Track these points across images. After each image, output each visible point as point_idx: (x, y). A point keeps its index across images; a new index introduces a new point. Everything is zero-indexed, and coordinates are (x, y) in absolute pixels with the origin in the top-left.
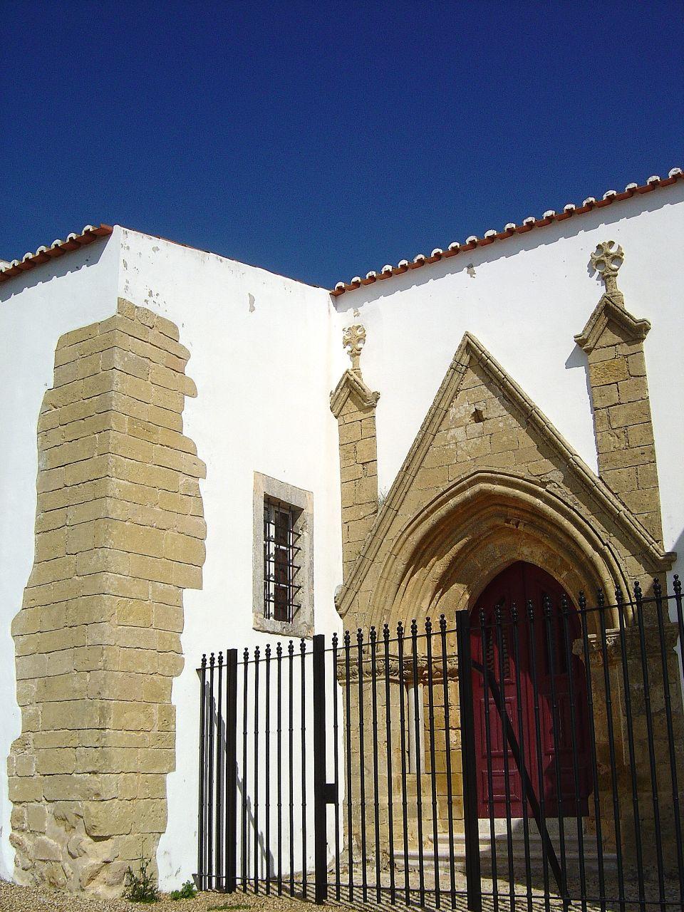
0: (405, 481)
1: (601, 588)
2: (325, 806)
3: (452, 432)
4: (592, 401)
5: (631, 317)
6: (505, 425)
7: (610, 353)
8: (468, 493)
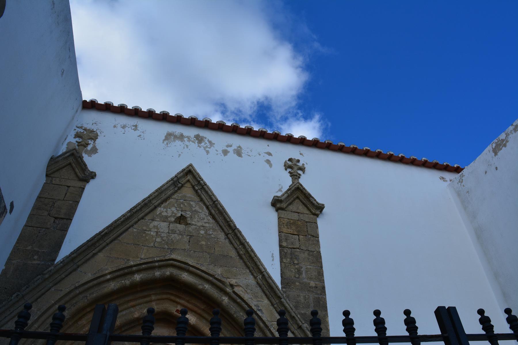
0: (97, 244)
1: (215, 200)
2: (139, 342)
3: (155, 223)
4: (280, 241)
5: (315, 200)
6: (206, 233)
7: (295, 216)
8: (157, 273)
